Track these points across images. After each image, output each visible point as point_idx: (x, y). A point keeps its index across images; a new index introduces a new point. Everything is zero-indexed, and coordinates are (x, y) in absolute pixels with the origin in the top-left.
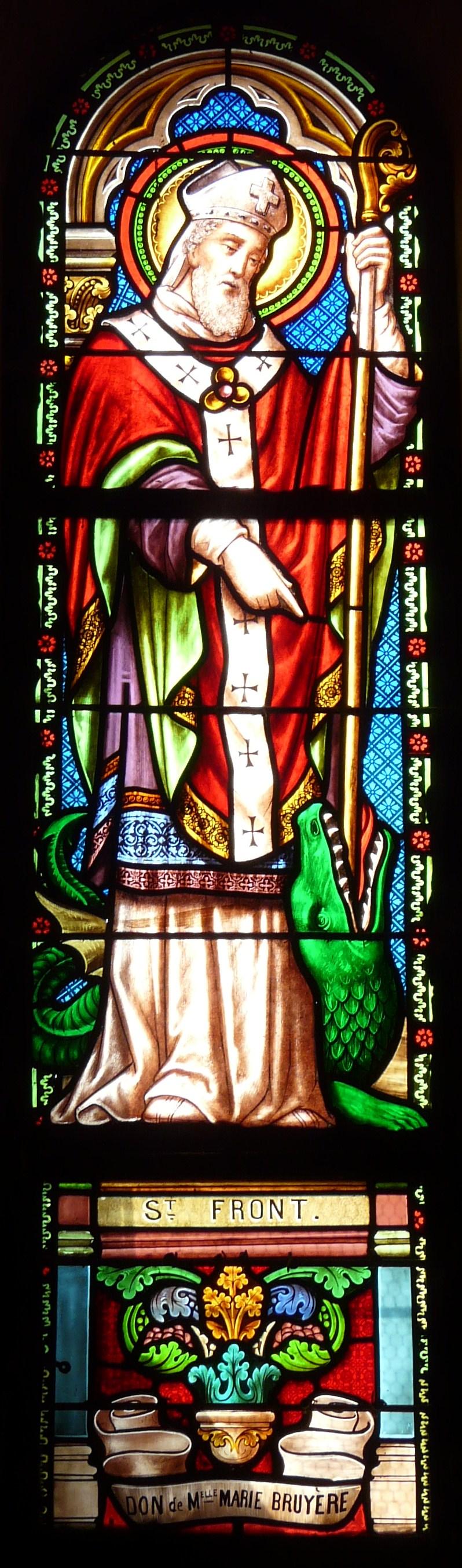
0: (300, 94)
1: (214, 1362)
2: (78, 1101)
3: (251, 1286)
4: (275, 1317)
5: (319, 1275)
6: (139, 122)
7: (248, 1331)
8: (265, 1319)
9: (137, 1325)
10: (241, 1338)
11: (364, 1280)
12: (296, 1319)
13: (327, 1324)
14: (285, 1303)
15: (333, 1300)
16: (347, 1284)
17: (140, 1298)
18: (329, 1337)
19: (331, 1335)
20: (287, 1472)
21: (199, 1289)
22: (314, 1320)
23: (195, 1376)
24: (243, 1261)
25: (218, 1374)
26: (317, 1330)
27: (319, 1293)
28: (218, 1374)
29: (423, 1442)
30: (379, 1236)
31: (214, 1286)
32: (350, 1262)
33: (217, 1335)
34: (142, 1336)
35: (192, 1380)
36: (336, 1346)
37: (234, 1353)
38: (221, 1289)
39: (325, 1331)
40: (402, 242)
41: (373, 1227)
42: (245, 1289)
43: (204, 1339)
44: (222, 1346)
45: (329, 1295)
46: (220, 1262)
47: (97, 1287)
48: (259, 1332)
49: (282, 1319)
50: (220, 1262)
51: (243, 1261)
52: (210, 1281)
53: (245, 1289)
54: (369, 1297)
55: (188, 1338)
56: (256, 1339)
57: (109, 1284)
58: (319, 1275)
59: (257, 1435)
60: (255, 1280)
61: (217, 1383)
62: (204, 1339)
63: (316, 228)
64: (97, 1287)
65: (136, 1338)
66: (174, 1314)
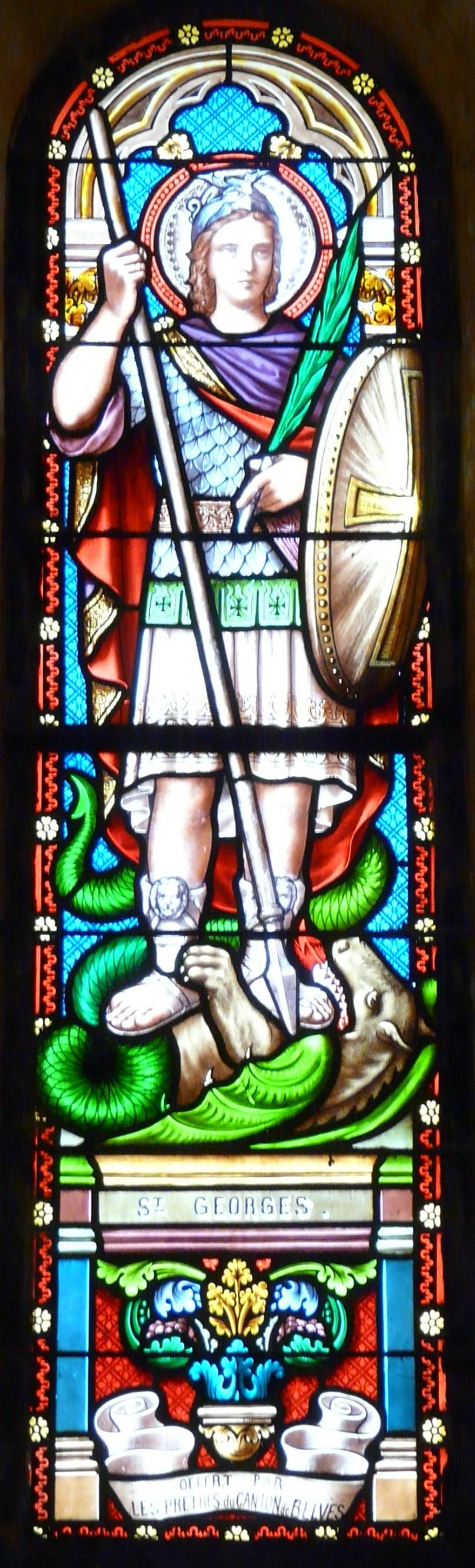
0: (308, 93)
1: (215, 1358)
2: (150, 99)
3: (256, 1281)
4: (278, 1312)
5: (322, 1273)
6: (138, 117)
7: (251, 1326)
8: (268, 1314)
9: (139, 1316)
10: (246, 1333)
11: (368, 1279)
12: (301, 1314)
13: (328, 1320)
14: (288, 1299)
15: (336, 1297)
16: (351, 1284)
17: (142, 1295)
18: (331, 1333)
19: (334, 1330)
20: (290, 1466)
21: (204, 1286)
22: (318, 1316)
23: (202, 1375)
24: (250, 1258)
25: (221, 1371)
26: (320, 1326)
27: (322, 1292)
28: (221, 1371)
29: (432, 804)
30: (383, 1231)
31: (218, 1282)
32: (354, 1259)
33: (220, 1331)
34: (145, 1328)
35: (195, 1376)
36: (337, 1343)
37: (237, 1346)
38: (225, 1286)
39: (327, 1327)
40: (404, 286)
41: (375, 1224)
42: (249, 1285)
43: (206, 1334)
44: (224, 1341)
45: (333, 1293)
46: (225, 1257)
47: (97, 1285)
48: (262, 1328)
49: (284, 1315)
50: (225, 1257)
51: (250, 1258)
52: (215, 1276)
53: (249, 1285)
54: (371, 1305)
55: (191, 1333)
56: (260, 1334)
57: (110, 1280)
58: (322, 1273)
59: (260, 1432)
60: (258, 1276)
61: (221, 1380)
62: (206, 1334)
63: (320, 247)
64: (97, 1285)
65: (138, 1330)
66: (178, 1309)
